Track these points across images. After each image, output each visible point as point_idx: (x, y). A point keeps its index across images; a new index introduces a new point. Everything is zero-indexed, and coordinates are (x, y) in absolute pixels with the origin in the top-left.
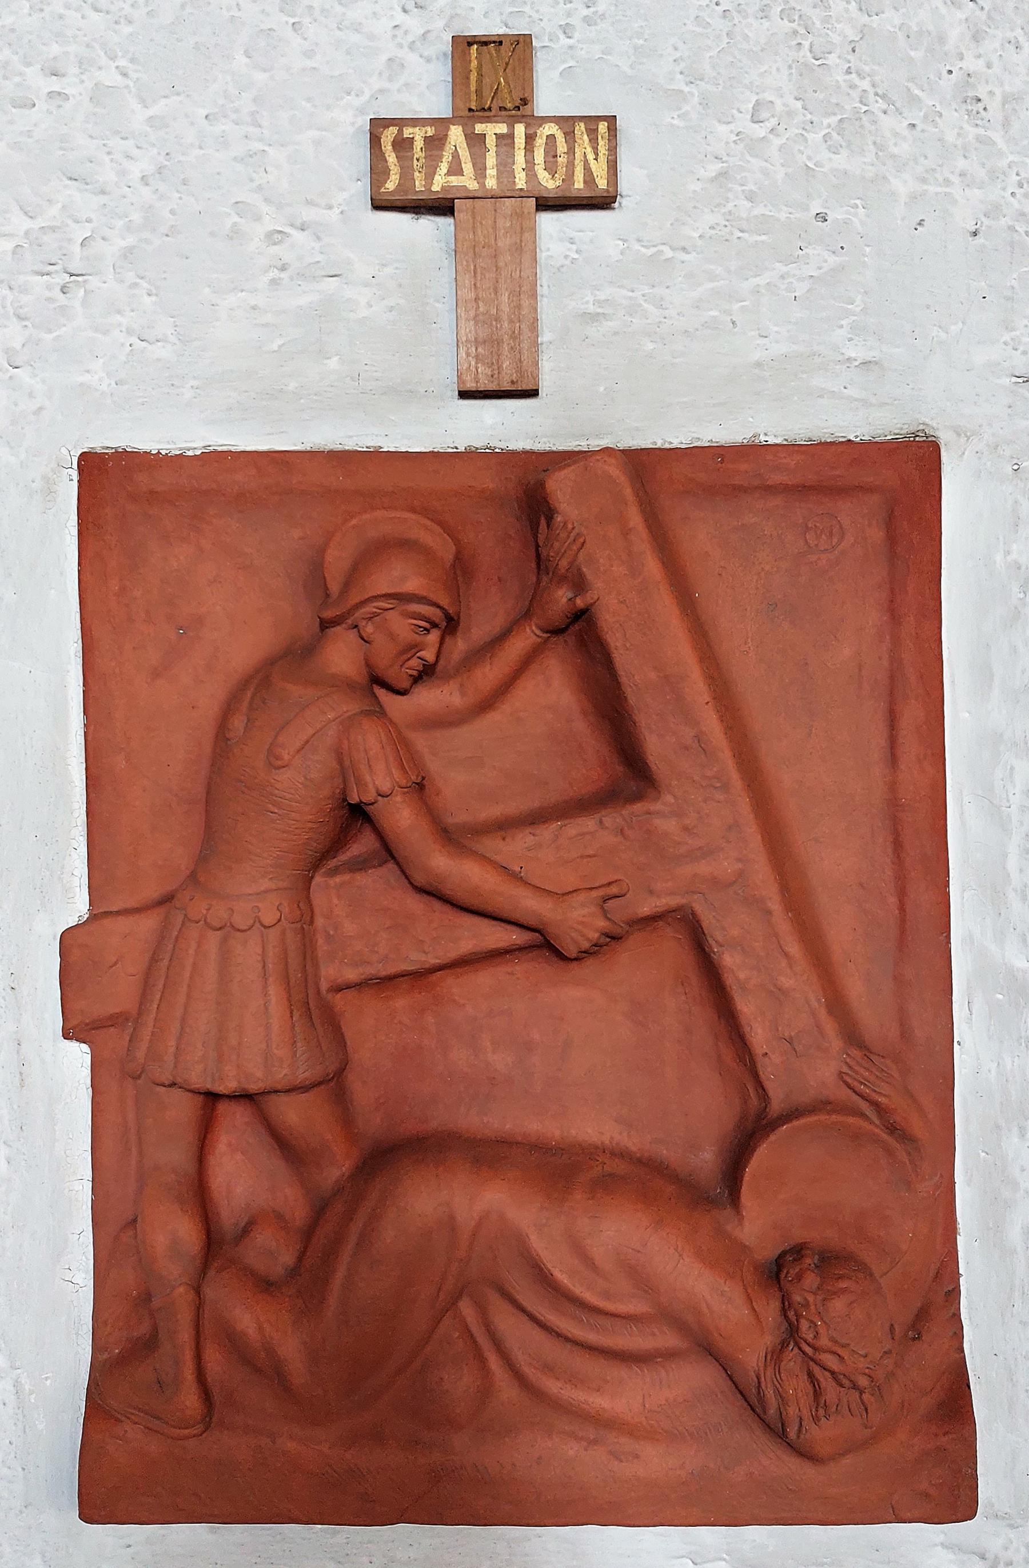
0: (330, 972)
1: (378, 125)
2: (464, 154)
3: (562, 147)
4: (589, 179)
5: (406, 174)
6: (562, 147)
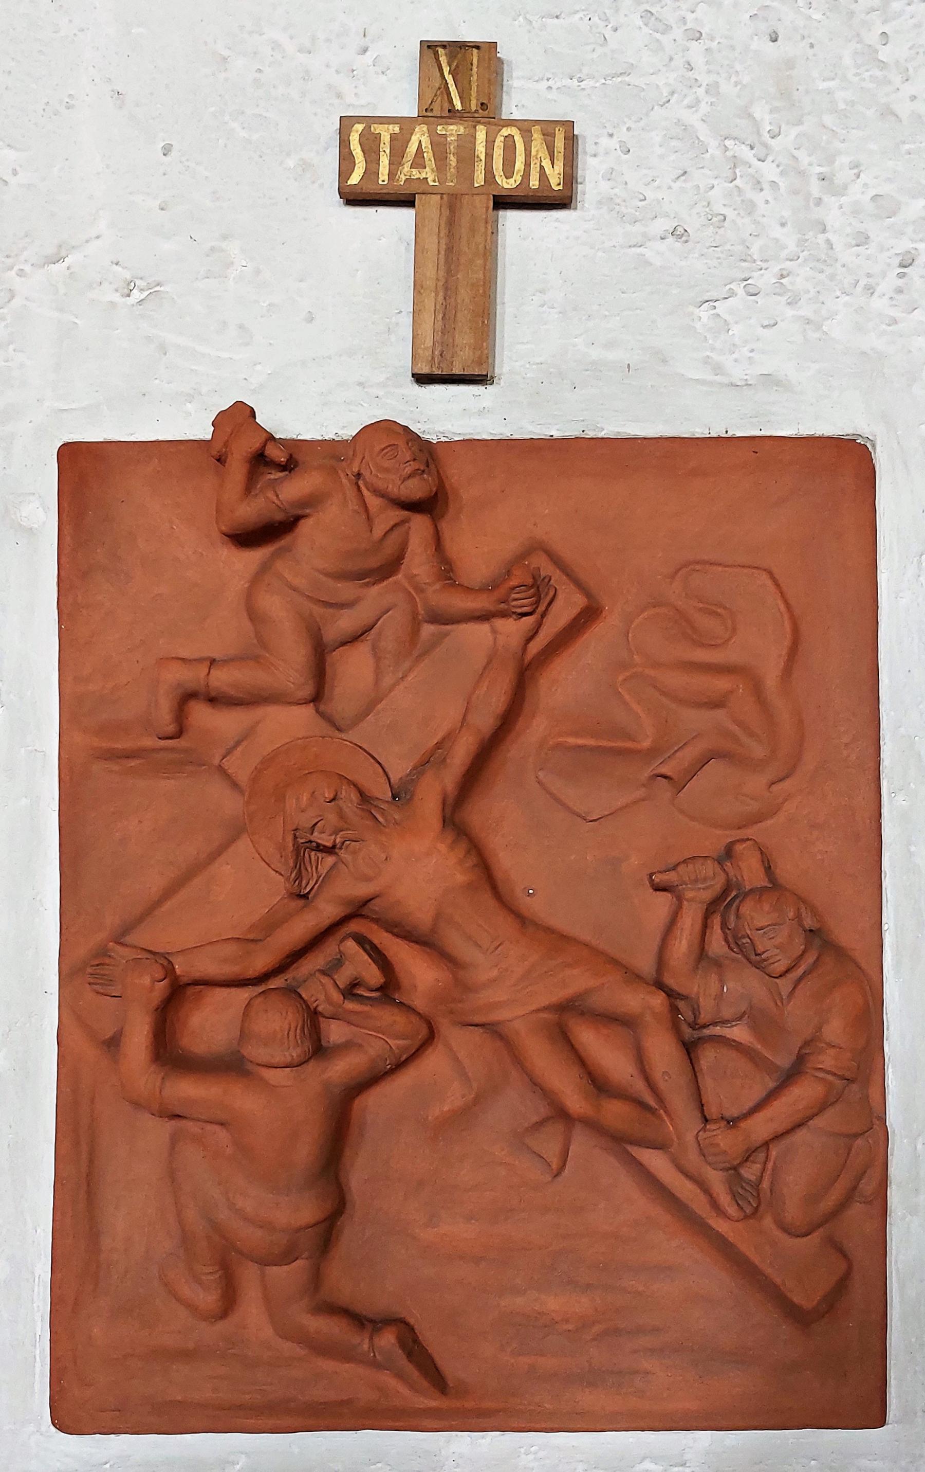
0: (230, 804)
2: (428, 155)
5: (371, 172)
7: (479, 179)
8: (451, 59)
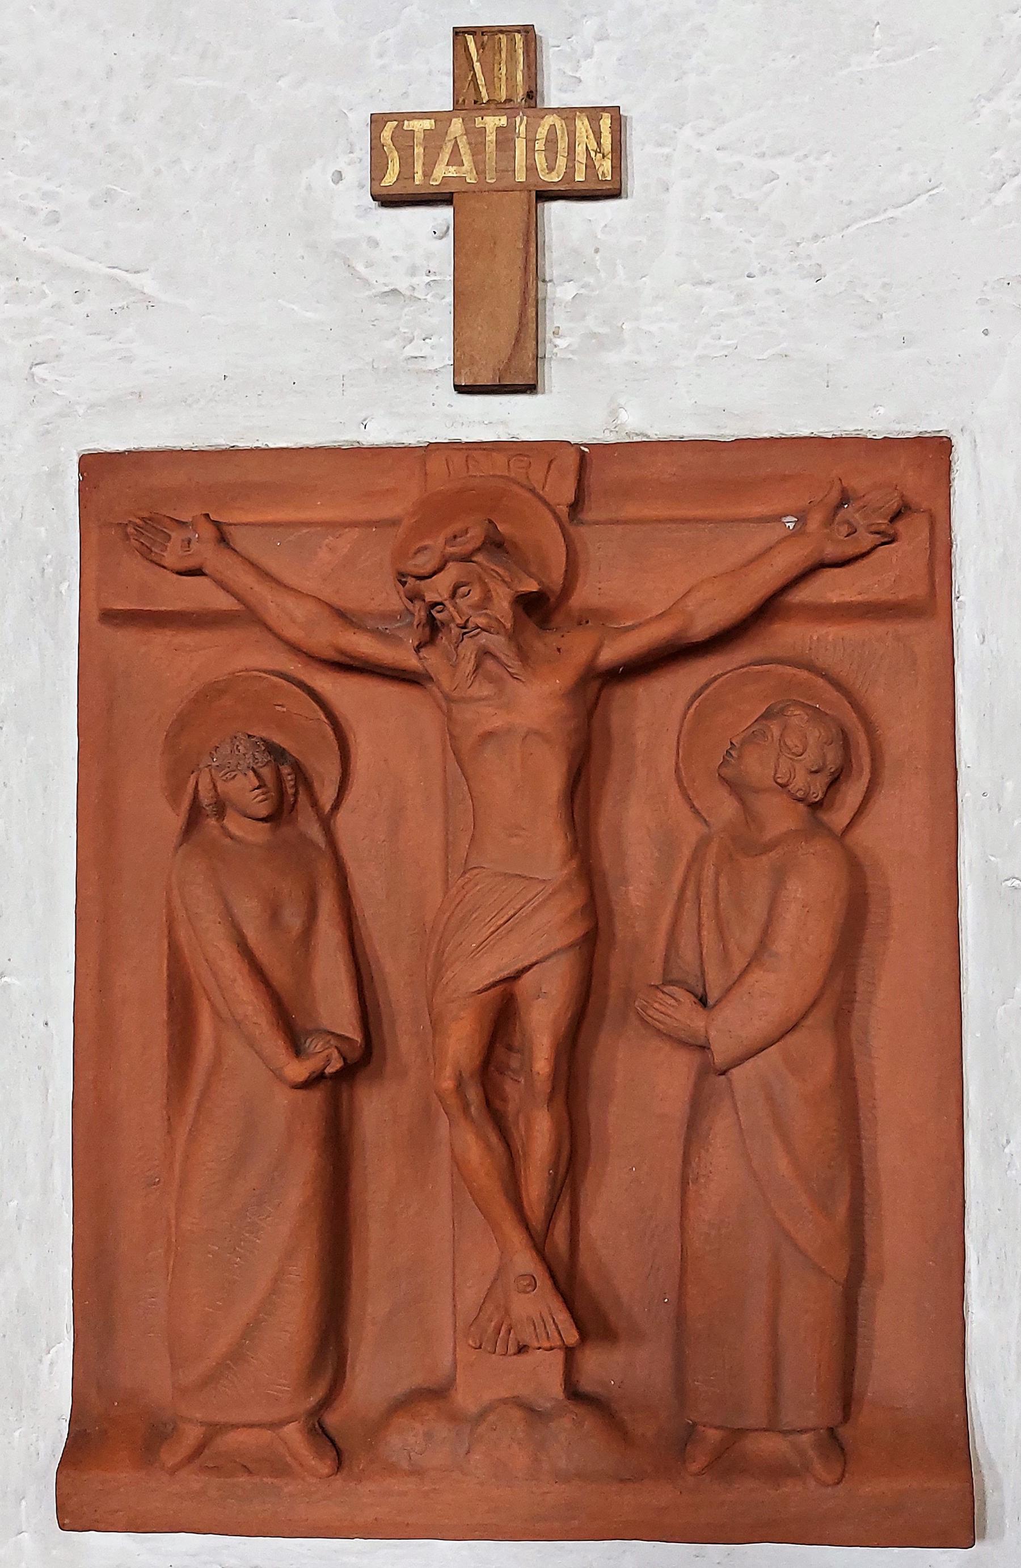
1: (377, 121)
3: (540, 160)
4: (590, 166)
6: (540, 160)
7: (521, 177)
8: (481, 46)
